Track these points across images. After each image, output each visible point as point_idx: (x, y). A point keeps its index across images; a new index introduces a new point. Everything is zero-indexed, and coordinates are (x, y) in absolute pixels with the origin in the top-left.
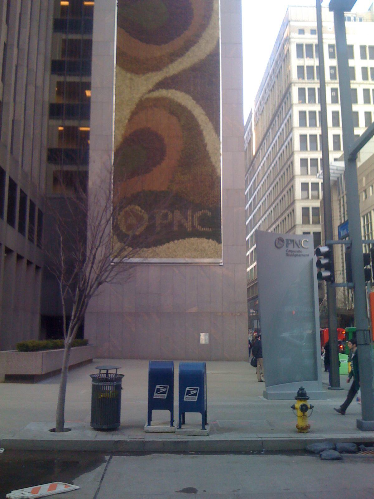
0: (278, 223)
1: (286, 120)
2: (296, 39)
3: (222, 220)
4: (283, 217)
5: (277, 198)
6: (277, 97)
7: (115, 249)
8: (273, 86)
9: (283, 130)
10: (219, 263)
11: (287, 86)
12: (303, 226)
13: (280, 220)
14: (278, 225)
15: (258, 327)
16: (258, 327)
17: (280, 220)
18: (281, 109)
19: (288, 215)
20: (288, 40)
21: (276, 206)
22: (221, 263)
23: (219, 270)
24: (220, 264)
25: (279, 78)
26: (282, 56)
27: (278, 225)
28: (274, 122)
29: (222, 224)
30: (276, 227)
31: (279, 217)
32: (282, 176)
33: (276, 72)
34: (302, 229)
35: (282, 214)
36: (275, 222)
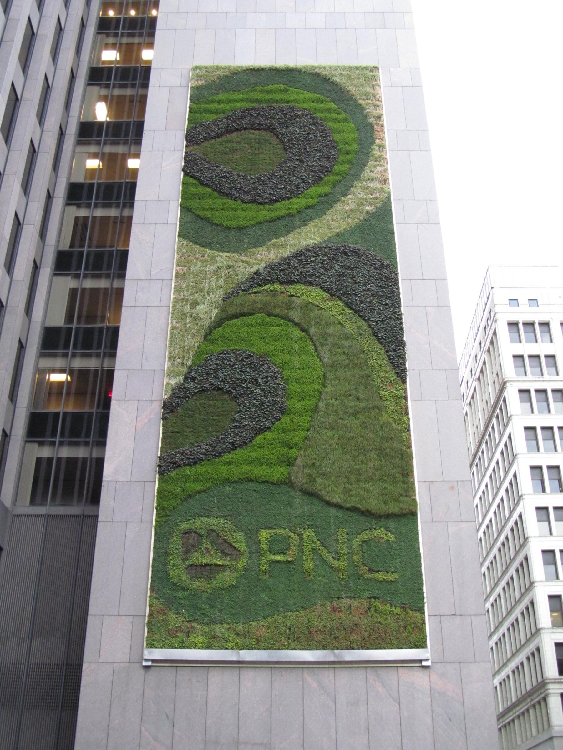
0: (503, 629)
1: (502, 446)
2: (506, 315)
3: (424, 577)
4: (512, 619)
5: (496, 585)
6: (471, 436)
7: (304, 105)
8: (473, 397)
9: (497, 463)
10: (421, 661)
11: (486, 417)
12: (555, 631)
13: (507, 624)
14: (504, 635)
15: (557, 726)
16: (557, 726)
17: (507, 624)
18: (490, 429)
19: (522, 614)
20: (492, 318)
21: (496, 600)
22: (427, 660)
23: (418, 678)
24: (424, 663)
25: (473, 407)
26: (475, 374)
27: (504, 635)
28: (480, 454)
29: (424, 582)
30: (500, 639)
31: (504, 619)
32: (503, 544)
33: (475, 374)
34: (553, 636)
35: (509, 613)
36: (497, 629)
